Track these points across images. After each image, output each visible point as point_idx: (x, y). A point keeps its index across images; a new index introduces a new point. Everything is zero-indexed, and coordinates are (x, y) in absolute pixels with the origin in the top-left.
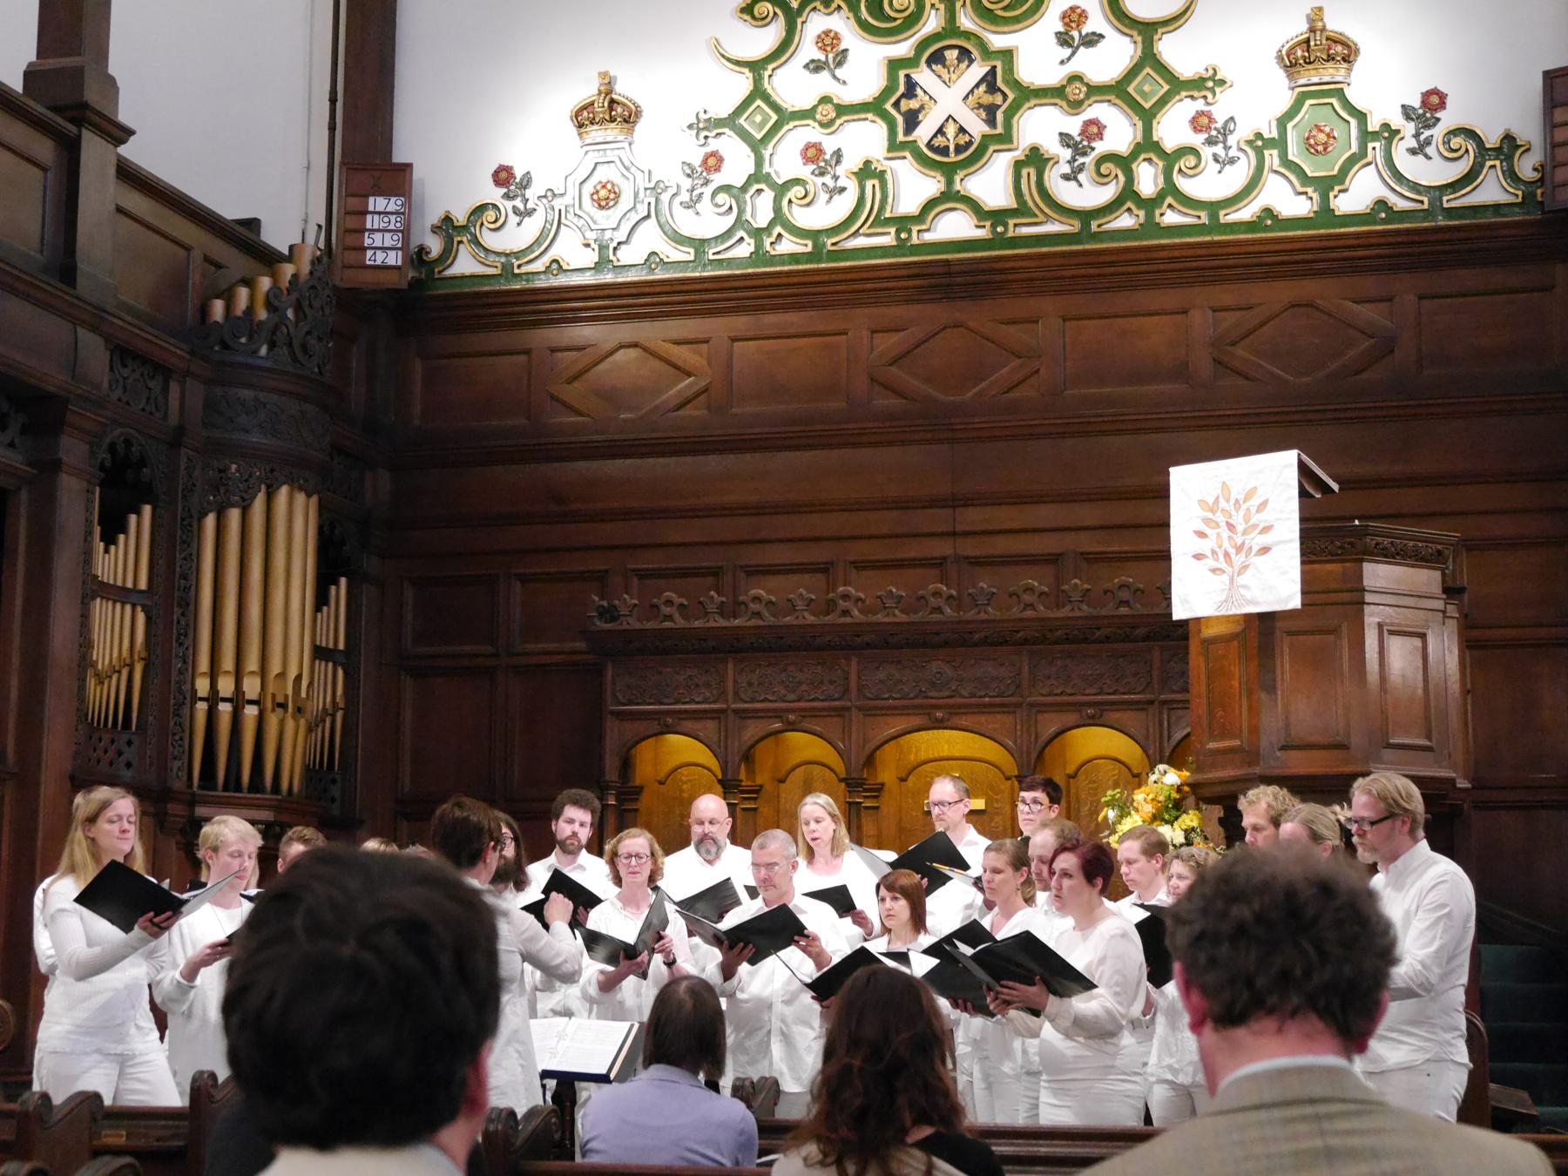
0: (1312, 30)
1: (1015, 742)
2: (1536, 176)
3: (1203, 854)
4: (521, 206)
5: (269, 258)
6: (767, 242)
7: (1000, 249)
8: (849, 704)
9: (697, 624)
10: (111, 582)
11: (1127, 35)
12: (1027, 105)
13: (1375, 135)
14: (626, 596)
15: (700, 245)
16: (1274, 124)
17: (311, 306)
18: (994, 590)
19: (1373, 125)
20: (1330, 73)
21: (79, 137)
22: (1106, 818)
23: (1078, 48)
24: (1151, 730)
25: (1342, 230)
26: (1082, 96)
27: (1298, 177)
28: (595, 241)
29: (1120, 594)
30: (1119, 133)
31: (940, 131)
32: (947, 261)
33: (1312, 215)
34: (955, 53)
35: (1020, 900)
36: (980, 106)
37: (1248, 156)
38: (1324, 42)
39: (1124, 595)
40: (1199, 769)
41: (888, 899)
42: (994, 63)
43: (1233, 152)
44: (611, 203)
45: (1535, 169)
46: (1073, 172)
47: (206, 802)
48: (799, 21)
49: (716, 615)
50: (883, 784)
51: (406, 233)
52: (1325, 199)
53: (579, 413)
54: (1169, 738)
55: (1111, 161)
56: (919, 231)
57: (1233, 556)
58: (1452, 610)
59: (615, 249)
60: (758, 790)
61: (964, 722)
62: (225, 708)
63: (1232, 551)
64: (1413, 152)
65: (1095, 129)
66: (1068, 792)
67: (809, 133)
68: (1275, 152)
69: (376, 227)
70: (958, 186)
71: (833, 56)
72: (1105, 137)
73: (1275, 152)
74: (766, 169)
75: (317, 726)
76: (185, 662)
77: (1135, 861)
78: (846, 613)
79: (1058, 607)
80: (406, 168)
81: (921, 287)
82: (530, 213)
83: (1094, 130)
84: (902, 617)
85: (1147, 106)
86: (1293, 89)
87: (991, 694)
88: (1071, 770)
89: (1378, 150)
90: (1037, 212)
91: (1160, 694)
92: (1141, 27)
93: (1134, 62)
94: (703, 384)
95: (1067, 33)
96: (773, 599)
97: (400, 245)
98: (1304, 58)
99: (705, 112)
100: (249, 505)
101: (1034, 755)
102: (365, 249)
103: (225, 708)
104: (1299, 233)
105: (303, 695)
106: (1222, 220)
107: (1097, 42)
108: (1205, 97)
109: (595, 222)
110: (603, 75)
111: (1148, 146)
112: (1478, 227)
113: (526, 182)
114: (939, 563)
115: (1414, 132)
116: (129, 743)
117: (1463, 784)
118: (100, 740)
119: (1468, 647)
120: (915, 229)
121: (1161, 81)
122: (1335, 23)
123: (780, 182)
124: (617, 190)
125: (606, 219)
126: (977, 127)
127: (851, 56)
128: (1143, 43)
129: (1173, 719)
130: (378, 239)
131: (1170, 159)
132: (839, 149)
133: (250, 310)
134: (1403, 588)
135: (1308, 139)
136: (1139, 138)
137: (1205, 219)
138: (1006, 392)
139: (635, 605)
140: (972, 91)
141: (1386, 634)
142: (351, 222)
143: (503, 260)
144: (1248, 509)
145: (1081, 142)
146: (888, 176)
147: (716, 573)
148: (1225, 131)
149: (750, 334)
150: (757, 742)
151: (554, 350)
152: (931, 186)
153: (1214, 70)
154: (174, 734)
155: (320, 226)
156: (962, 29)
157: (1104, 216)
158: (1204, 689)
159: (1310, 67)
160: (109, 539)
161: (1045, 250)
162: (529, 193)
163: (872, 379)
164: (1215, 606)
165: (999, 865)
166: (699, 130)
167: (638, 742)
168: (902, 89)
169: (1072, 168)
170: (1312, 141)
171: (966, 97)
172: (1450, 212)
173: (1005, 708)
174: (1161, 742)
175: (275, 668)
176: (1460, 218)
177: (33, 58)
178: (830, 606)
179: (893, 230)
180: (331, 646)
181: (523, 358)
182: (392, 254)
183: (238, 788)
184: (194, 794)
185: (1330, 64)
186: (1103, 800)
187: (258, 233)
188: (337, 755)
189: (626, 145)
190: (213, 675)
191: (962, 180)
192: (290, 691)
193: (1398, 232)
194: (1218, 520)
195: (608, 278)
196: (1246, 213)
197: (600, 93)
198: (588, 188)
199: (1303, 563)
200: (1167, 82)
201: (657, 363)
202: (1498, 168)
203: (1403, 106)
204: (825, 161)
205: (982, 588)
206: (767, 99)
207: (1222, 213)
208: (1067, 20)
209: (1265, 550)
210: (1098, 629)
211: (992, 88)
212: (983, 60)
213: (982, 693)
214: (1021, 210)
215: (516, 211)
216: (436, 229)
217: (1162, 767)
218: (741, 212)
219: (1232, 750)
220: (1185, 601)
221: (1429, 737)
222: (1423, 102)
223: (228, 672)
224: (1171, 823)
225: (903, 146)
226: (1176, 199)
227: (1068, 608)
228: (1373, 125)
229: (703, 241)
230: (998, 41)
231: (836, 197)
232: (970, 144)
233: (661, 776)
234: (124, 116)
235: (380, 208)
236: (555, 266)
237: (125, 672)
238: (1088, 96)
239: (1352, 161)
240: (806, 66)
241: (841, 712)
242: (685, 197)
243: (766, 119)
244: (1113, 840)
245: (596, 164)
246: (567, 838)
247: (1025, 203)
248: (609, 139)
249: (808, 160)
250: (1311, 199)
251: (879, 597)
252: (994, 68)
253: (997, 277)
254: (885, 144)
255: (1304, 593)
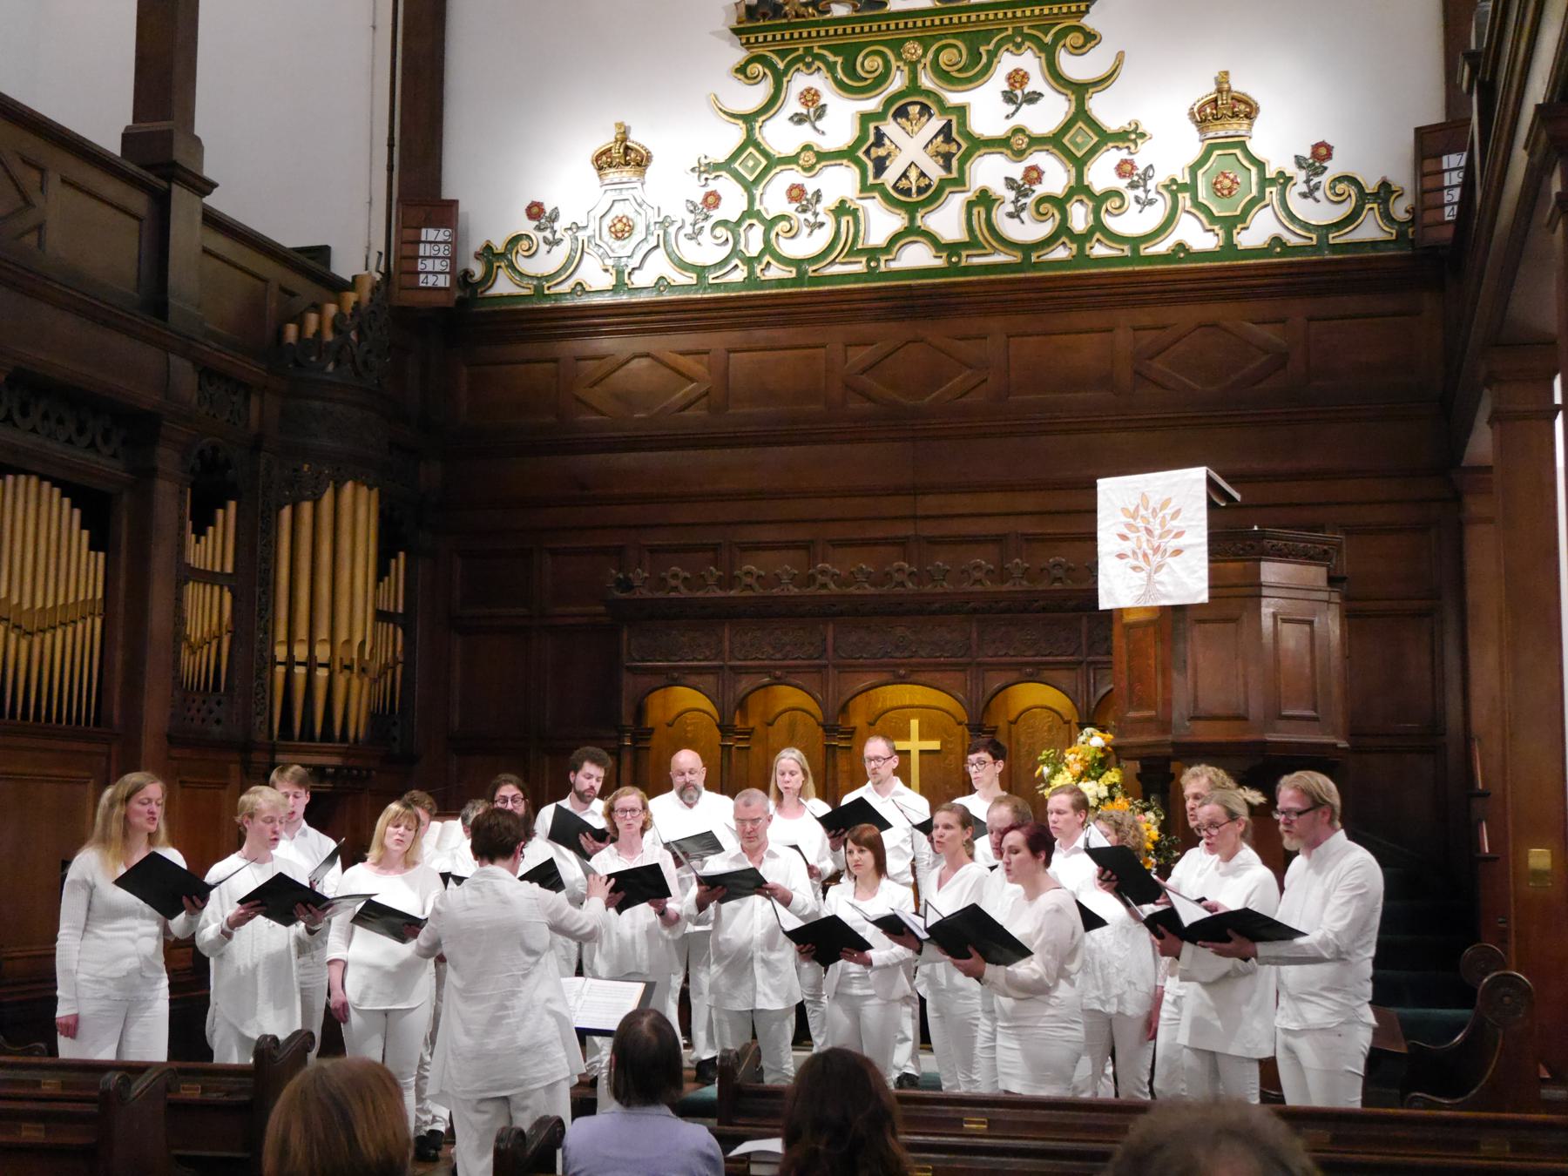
0: (1220, 91)
1: (966, 696)
2: (1407, 217)
3: (1121, 815)
4: (550, 236)
5: (338, 287)
6: (758, 269)
7: (955, 276)
8: (824, 662)
9: (700, 594)
10: (202, 567)
11: (1063, 94)
12: (978, 153)
13: (1272, 182)
14: (639, 570)
15: (701, 271)
16: (1187, 171)
17: (370, 327)
18: (948, 568)
19: (1271, 172)
20: (1235, 128)
21: (169, 191)
22: (1041, 774)
23: (1021, 105)
24: (1080, 687)
25: (1244, 262)
26: (1024, 146)
27: (1207, 217)
28: (613, 267)
29: (1055, 572)
30: (1056, 178)
31: (904, 175)
32: (910, 286)
33: (1218, 249)
34: (917, 109)
35: (965, 856)
36: (938, 154)
37: (1164, 199)
38: (1229, 101)
39: (1059, 573)
40: (1119, 733)
41: (856, 852)
42: (950, 117)
43: (1152, 195)
44: (626, 235)
45: (1407, 211)
46: (1016, 211)
47: (287, 751)
48: (785, 80)
49: (715, 588)
50: (855, 728)
51: (453, 259)
52: (1229, 236)
53: (598, 412)
54: (1095, 692)
55: (1048, 202)
56: (886, 261)
57: (1150, 557)
58: (1335, 598)
59: (630, 274)
60: (749, 733)
61: (923, 677)
62: (300, 671)
63: (1150, 552)
64: (1304, 195)
65: (1035, 175)
66: (1010, 752)
67: (792, 176)
68: (1187, 195)
69: (428, 254)
70: (919, 222)
71: (814, 110)
72: (1043, 181)
73: (1187, 195)
74: (757, 206)
75: (380, 677)
76: (266, 633)
77: (1065, 812)
78: (824, 586)
79: (1003, 582)
80: (454, 203)
81: (888, 308)
82: (557, 242)
83: (1033, 175)
84: (871, 590)
85: (1079, 154)
86: (1203, 141)
87: (946, 655)
88: (1012, 717)
89: (1274, 194)
90: (987, 246)
91: (1089, 655)
92: (1074, 87)
93: (1068, 117)
94: (703, 389)
95: (1011, 92)
96: (763, 573)
97: (448, 270)
98: (1213, 115)
99: (706, 157)
100: (320, 499)
101: (982, 706)
102: (419, 273)
103: (300, 671)
104: (1207, 264)
105: (367, 657)
106: (1143, 253)
107: (1037, 99)
108: (1128, 148)
109: (613, 251)
110: (619, 125)
111: (1079, 189)
112: (1361, 260)
113: (554, 217)
114: (901, 543)
115: (1305, 179)
116: (219, 703)
117: (1343, 744)
118: (194, 701)
119: (1347, 616)
120: (883, 259)
121: (1091, 134)
122: (1238, 85)
123: (769, 218)
124: (631, 223)
125: (622, 248)
126: (935, 172)
127: (829, 110)
128: (1076, 100)
129: (1098, 677)
130: (429, 265)
131: (1100, 201)
132: (819, 190)
133: (319, 333)
134: (1294, 583)
135: (1215, 184)
136: (1073, 183)
137: (1128, 252)
138: (960, 397)
139: (646, 578)
140: (931, 141)
141: (1279, 623)
142: (407, 250)
143: (535, 283)
144: (1164, 517)
145: (1023, 186)
146: (861, 214)
147: (715, 548)
148: (1146, 177)
149: (745, 346)
150: (750, 693)
151: (578, 359)
152: (897, 222)
153: (1136, 124)
154: (257, 694)
155: (380, 254)
156: (923, 88)
157: (1043, 249)
158: (1125, 666)
159: (1218, 122)
160: (200, 531)
161: (992, 277)
162: (557, 226)
163: (847, 386)
164: (1135, 599)
165: (951, 822)
166: (700, 172)
167: (651, 692)
168: (872, 139)
169: (1016, 207)
170: (1219, 186)
171: (926, 146)
172: (1335, 248)
173: (961, 667)
174: (1088, 696)
175: (342, 636)
176: (1342, 253)
177: (130, 122)
178: (811, 580)
179: (864, 260)
180: (392, 610)
181: (551, 366)
182: (441, 277)
183: (312, 738)
184: (274, 745)
185: (1234, 120)
186: (1039, 758)
187: (327, 263)
188: (397, 703)
189: (638, 185)
190: (290, 644)
191: (922, 217)
192: (355, 656)
193: (1291, 264)
194: (1139, 525)
195: (624, 298)
196: (1162, 247)
197: (616, 141)
198: (607, 221)
199: (1210, 561)
200: (1096, 134)
201: (667, 371)
202: (1376, 210)
203: (1296, 156)
204: (807, 200)
205: (938, 566)
206: (757, 146)
207: (1142, 247)
208: (1012, 81)
209: (1178, 552)
210: (1037, 601)
211: (949, 139)
212: (941, 114)
213: (938, 654)
214: (972, 243)
215: (546, 240)
216: (478, 256)
217: (1089, 730)
218: (736, 243)
219: (1149, 720)
220: (1110, 594)
221: (1315, 709)
222: (1313, 153)
223: (302, 641)
224: (1097, 779)
225: (873, 187)
226: (1103, 234)
227: (1011, 582)
228: (1271, 172)
229: (704, 268)
230: (953, 98)
231: (816, 231)
232: (929, 186)
233: (670, 718)
234: (208, 172)
235: (431, 238)
236: (579, 288)
237: (214, 643)
238: (1029, 145)
239: (1253, 203)
240: (791, 119)
241: (820, 669)
242: (688, 229)
243: (757, 163)
244: (1047, 792)
245: (614, 201)
246: (586, 791)
247: (976, 237)
248: (625, 180)
249: (792, 199)
250: (1217, 235)
251: (852, 573)
252: (950, 121)
253: (954, 300)
254: (858, 185)
255: (1211, 587)
